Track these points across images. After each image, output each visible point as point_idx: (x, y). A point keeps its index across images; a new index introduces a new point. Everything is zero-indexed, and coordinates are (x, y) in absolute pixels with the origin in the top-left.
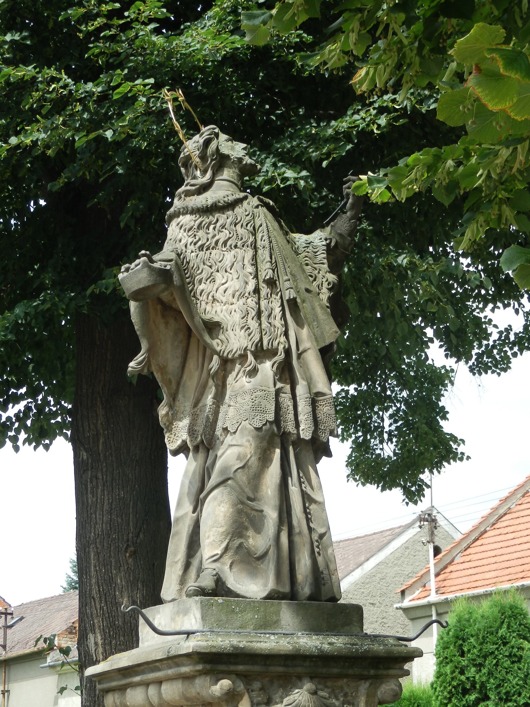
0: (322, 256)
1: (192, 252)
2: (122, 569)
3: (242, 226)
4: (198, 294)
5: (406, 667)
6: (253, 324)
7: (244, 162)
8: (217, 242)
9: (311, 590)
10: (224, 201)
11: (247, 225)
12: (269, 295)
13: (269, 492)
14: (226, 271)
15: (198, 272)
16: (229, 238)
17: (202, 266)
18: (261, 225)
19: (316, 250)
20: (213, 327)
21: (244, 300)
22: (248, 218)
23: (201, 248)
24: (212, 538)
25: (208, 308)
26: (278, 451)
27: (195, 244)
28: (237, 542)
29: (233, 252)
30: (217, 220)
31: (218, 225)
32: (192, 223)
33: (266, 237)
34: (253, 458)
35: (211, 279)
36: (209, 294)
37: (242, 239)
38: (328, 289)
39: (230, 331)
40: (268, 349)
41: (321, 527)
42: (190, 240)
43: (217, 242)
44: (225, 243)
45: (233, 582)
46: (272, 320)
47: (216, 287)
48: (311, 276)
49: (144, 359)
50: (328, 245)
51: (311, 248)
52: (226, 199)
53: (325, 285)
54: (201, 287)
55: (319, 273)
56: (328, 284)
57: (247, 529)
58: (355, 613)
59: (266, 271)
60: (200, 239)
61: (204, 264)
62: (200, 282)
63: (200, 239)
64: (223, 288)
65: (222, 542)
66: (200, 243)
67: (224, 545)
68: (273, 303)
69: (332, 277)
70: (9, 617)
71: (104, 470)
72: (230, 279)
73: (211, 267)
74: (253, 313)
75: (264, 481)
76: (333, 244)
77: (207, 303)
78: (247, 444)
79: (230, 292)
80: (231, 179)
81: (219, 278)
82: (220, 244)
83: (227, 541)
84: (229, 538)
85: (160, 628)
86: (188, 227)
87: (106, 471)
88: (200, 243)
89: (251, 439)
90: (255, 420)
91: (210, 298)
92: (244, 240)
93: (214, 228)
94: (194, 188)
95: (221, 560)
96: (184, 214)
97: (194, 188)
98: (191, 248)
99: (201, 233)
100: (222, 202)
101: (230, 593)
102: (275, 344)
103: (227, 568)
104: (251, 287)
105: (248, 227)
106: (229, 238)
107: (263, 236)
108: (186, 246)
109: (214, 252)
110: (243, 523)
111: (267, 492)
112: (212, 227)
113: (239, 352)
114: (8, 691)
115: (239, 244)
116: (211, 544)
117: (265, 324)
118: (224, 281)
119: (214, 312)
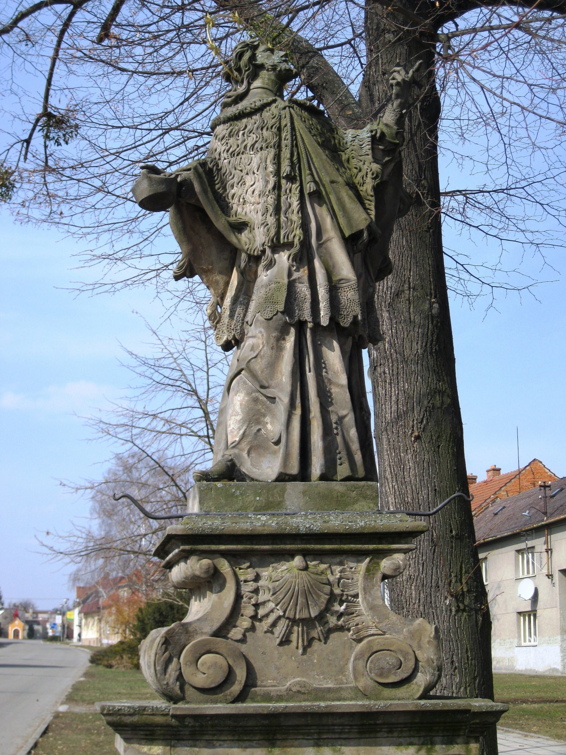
0: (367, 147)
1: (225, 159)
2: (409, 451)
3: (267, 129)
4: (230, 197)
7: (279, 69)
8: (245, 147)
9: (322, 470)
10: (251, 108)
11: (272, 127)
12: (288, 191)
13: (284, 380)
14: (254, 173)
15: (231, 177)
16: (256, 142)
17: (233, 171)
18: (286, 126)
19: (361, 143)
20: (240, 227)
21: (265, 198)
22: (274, 120)
23: (232, 154)
25: (240, 210)
27: (228, 151)
28: (255, 429)
30: (246, 127)
32: (224, 132)
34: (265, 348)
35: (242, 182)
36: (240, 196)
37: (266, 141)
38: (373, 179)
39: (256, 229)
40: (284, 243)
41: (344, 410)
43: (245, 147)
44: (253, 145)
45: (251, 467)
46: (289, 215)
47: (246, 189)
48: (356, 168)
49: (184, 263)
51: (356, 141)
52: (253, 106)
53: (370, 175)
54: (233, 191)
55: (364, 164)
56: (373, 174)
57: (264, 416)
59: (286, 169)
60: (231, 147)
61: (235, 169)
62: (232, 186)
63: (231, 147)
64: (251, 189)
67: (241, 432)
68: (292, 199)
69: (376, 167)
70: (547, 489)
71: (390, 365)
72: (257, 180)
73: (241, 171)
74: (271, 209)
75: (280, 368)
76: (378, 135)
77: (238, 205)
78: (260, 335)
79: (257, 192)
80: (266, 86)
81: (249, 180)
83: (244, 428)
84: (246, 425)
87: (392, 366)
89: (263, 330)
90: (266, 312)
91: (241, 200)
92: (268, 141)
93: (243, 134)
94: (230, 99)
95: (239, 446)
96: (219, 125)
97: (230, 99)
98: (224, 155)
99: (232, 141)
100: (249, 108)
101: (242, 477)
102: (291, 237)
103: (245, 454)
105: (273, 130)
106: (256, 142)
107: (286, 136)
108: (220, 154)
109: (243, 156)
110: (259, 410)
111: (281, 380)
112: (241, 133)
114: (551, 550)
115: (264, 145)
117: (283, 218)
118: (252, 183)
119: (244, 213)
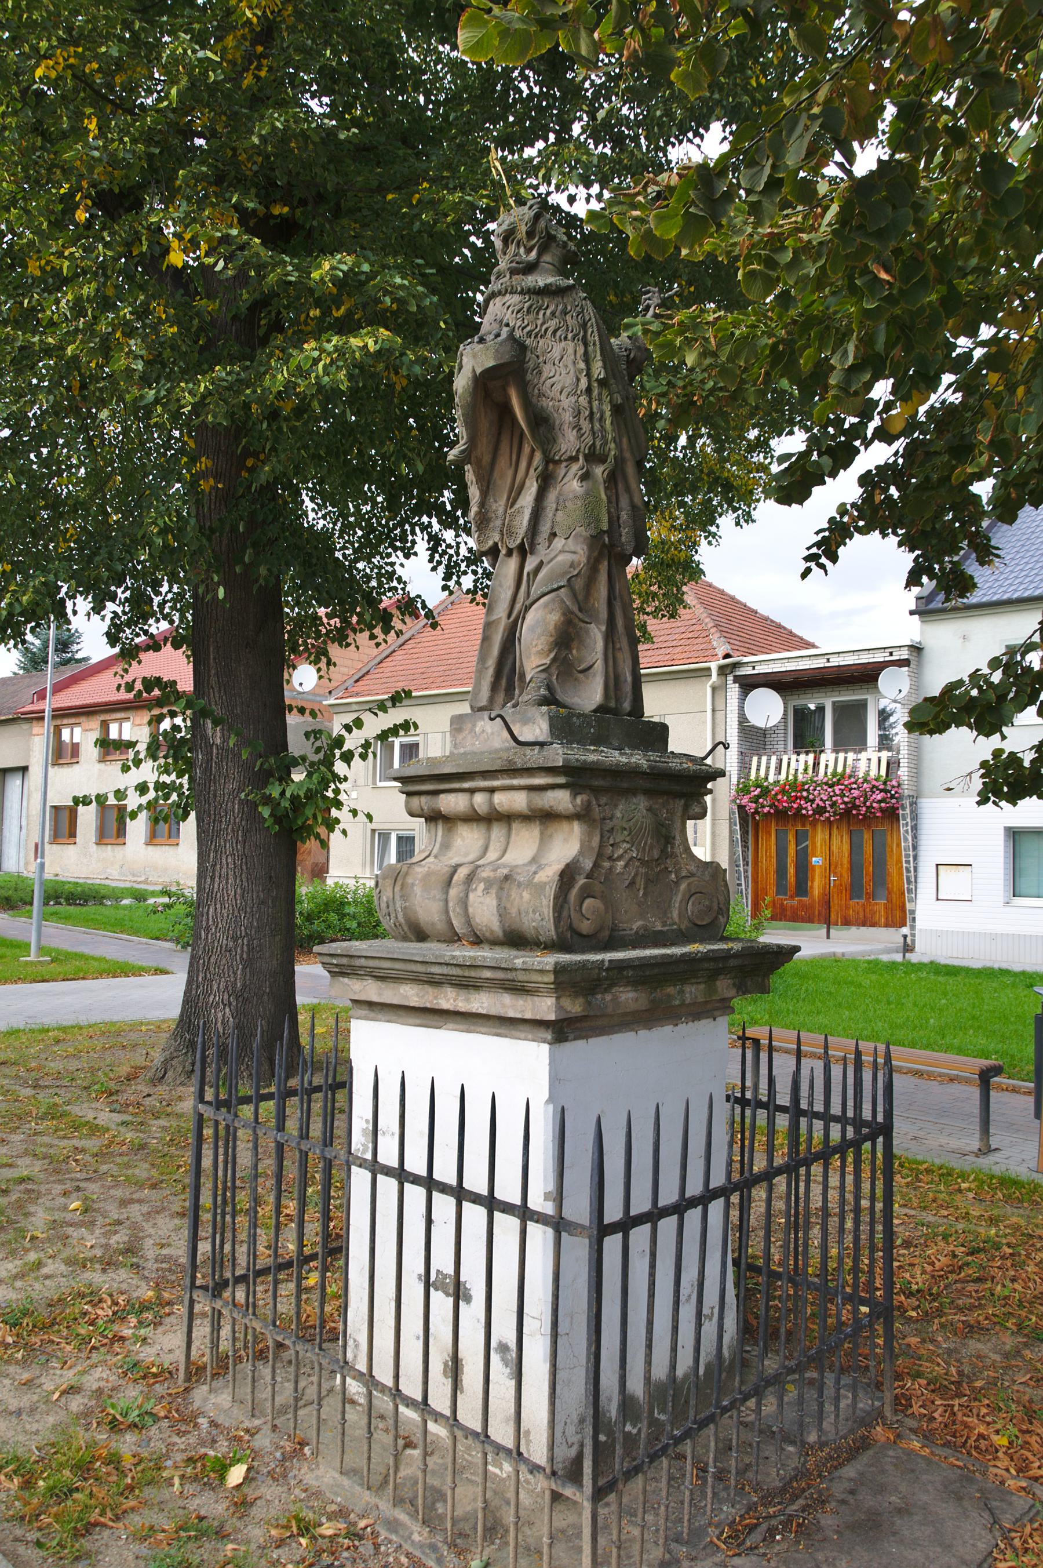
5: (709, 786)
6: (585, 425)
24: (540, 647)
26: (606, 563)
29: (563, 343)
31: (548, 312)
33: (596, 333)
42: (519, 323)
50: (628, 356)
58: (660, 732)
65: (550, 651)
66: (528, 328)
67: (552, 655)
82: (549, 333)
85: (521, 739)
86: (517, 308)
88: (528, 328)
104: (584, 383)
113: (568, 454)
116: (539, 653)
117: (597, 426)
